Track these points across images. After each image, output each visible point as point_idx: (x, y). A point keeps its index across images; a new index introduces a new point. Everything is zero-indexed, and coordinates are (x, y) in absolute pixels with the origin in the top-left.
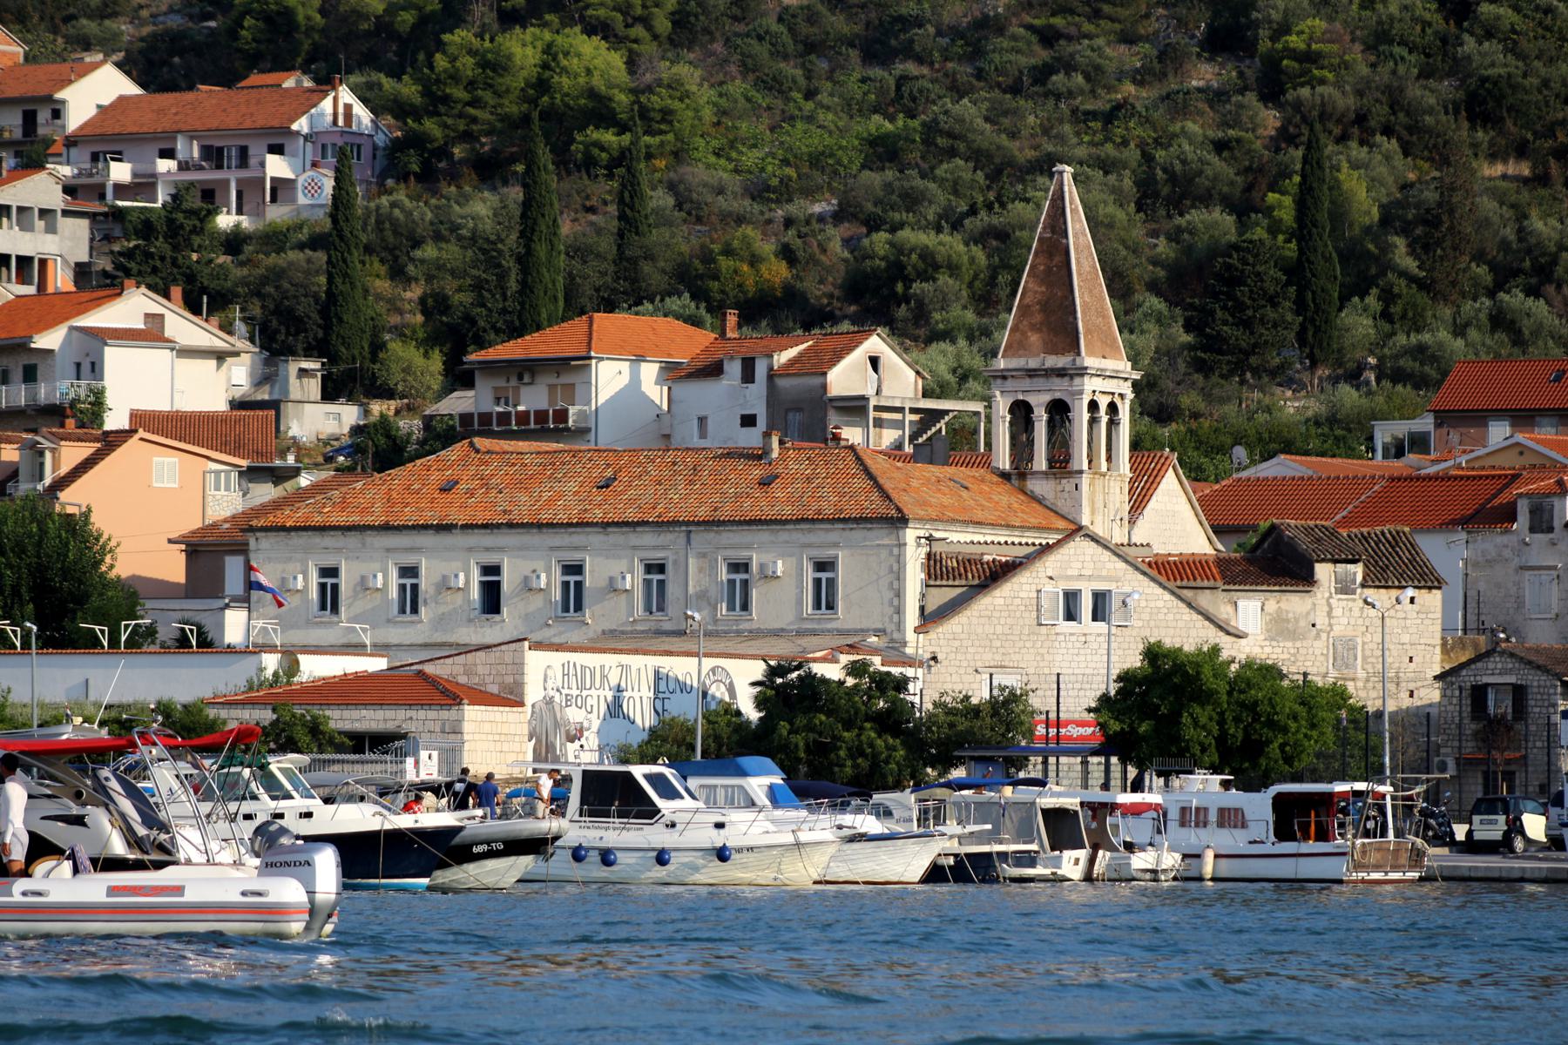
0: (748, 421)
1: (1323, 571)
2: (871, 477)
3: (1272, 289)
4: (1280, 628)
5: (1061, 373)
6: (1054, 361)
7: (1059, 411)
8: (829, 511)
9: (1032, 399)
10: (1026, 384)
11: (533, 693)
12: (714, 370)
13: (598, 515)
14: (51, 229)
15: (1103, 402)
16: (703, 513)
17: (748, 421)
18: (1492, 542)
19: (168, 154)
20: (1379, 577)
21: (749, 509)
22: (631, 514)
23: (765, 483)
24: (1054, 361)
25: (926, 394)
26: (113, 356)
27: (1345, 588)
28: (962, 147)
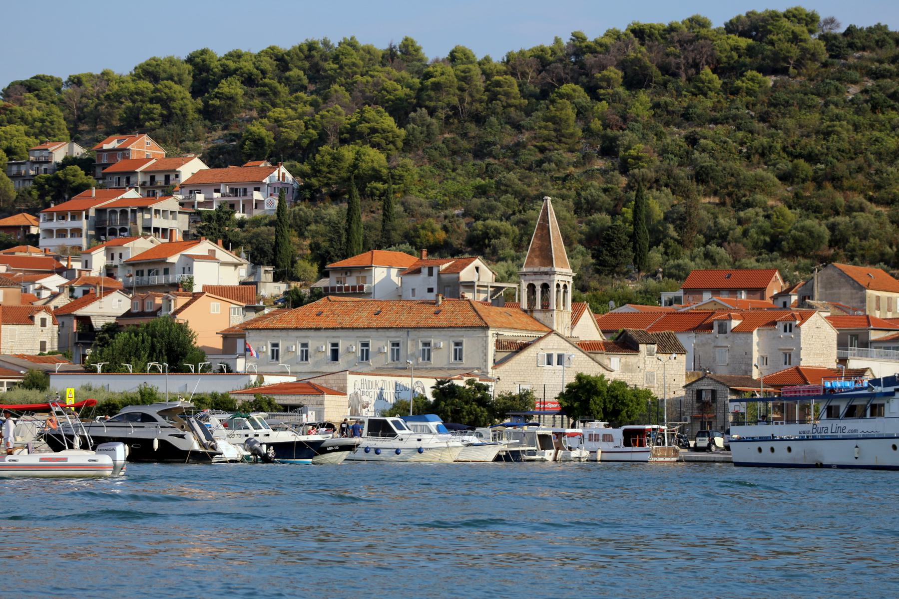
0: (430, 290)
1: (642, 347)
2: (476, 311)
4: (626, 368)
5: (546, 273)
7: (545, 287)
8: (460, 324)
9: (535, 283)
10: (533, 277)
11: (350, 391)
13: (374, 325)
14: (174, 218)
15: (538, 285)
16: (413, 324)
17: (430, 290)
19: (217, 191)
20: (663, 349)
21: (430, 323)
22: (387, 325)
23: (436, 313)
24: (544, 269)
25: (496, 281)
26: (197, 266)
27: (650, 354)
28: (510, 190)
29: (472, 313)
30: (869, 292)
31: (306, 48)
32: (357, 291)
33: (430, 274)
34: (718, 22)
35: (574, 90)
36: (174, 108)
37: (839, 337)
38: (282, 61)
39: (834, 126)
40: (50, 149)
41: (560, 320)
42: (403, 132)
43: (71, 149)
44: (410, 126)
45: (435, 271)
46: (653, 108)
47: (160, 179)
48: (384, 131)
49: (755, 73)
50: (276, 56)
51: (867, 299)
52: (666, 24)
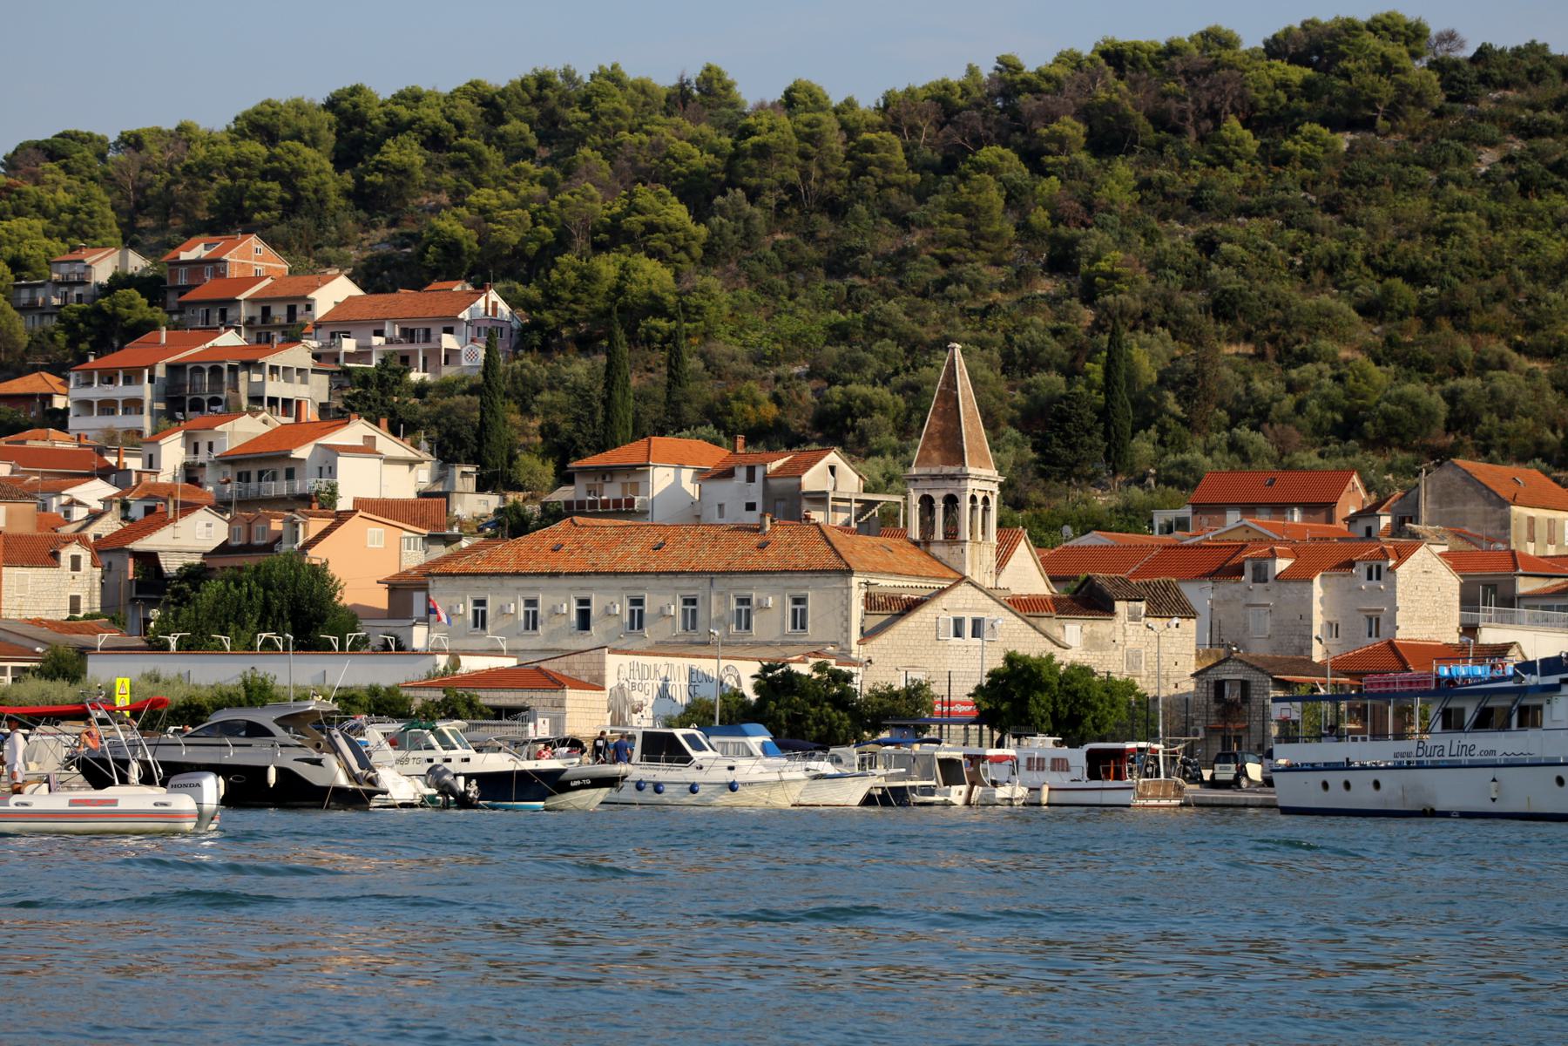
0: (751, 507)
1: (1121, 606)
2: (829, 543)
3: (1088, 425)
4: (1092, 642)
5: (952, 477)
6: (948, 470)
7: (951, 501)
8: (802, 566)
9: (934, 494)
10: (930, 484)
11: (611, 682)
12: (728, 474)
13: (653, 567)
14: (304, 381)
15: (938, 497)
16: (721, 566)
17: (751, 507)
18: (1228, 588)
19: (379, 333)
20: (1156, 610)
21: (750, 563)
22: (675, 567)
23: (761, 547)
24: (948, 470)
25: (866, 490)
26: (344, 464)
27: (1134, 617)
29: (823, 547)
30: (1515, 509)
31: (533, 84)
32: (623, 509)
33: (751, 478)
34: (1252, 38)
35: (1001, 158)
36: (304, 189)
37: (1464, 589)
38: (491, 106)
39: (1454, 220)
40: (88, 261)
41: (977, 558)
42: (702, 231)
43: (124, 259)
44: (716, 220)
45: (759, 473)
46: (1139, 188)
47: (279, 313)
48: (670, 229)
49: (1316, 127)
50: (482, 97)
51: (1513, 522)
52: (1162, 42)
